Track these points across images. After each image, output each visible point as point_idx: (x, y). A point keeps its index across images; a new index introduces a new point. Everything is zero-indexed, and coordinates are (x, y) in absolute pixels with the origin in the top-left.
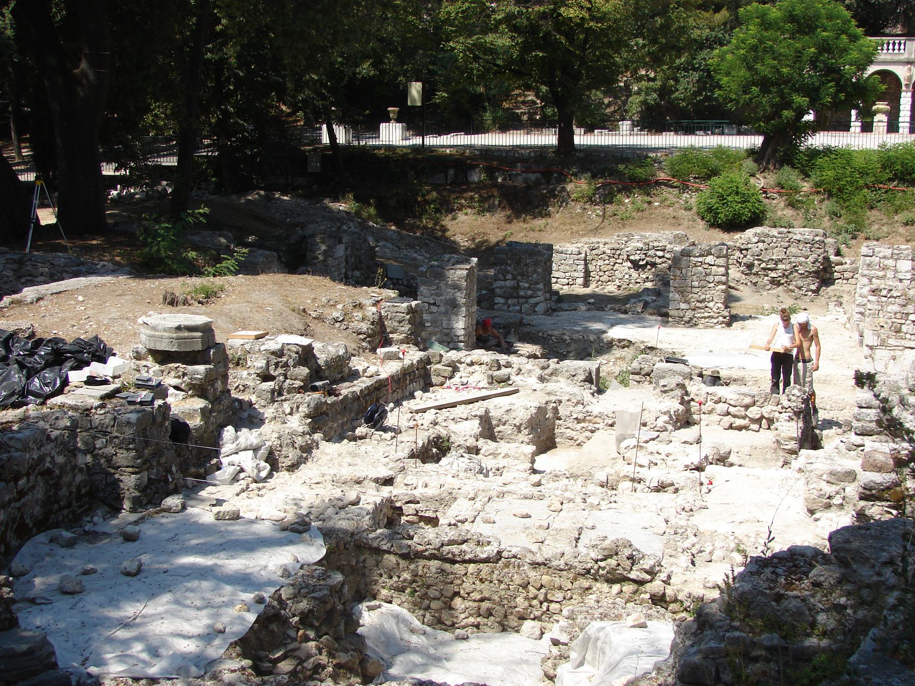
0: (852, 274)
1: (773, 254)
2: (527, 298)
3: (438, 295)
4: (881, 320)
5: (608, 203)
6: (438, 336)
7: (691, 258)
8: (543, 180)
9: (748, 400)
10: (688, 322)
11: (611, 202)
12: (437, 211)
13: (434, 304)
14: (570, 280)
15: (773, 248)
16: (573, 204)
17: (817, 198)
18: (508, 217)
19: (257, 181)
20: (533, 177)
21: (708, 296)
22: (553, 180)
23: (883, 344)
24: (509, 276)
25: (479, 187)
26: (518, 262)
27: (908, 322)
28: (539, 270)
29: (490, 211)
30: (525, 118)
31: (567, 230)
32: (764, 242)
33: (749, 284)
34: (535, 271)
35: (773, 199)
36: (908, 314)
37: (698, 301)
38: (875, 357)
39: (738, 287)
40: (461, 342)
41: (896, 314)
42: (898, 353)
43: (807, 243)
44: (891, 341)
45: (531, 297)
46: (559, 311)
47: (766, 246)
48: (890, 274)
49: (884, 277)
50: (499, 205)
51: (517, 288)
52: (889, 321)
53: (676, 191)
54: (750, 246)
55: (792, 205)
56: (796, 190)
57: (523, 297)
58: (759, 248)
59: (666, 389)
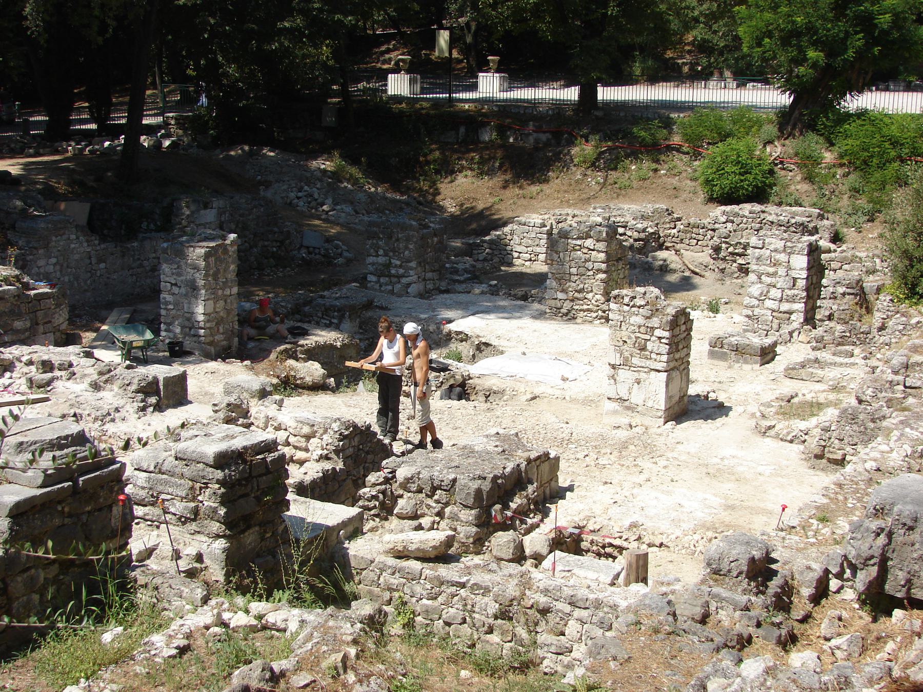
0: (840, 264)
1: (742, 237)
2: (399, 277)
3: (179, 275)
4: (624, 333)
5: (612, 170)
6: (180, 320)
7: (569, 241)
8: (553, 141)
9: (306, 430)
10: (566, 314)
11: (615, 169)
12: (438, 172)
13: (176, 285)
14: (532, 255)
15: (743, 230)
16: (574, 169)
17: (840, 172)
18: (506, 181)
19: (278, 133)
20: (544, 137)
21: (586, 286)
22: (563, 142)
23: (626, 363)
24: (381, 252)
25: (490, 145)
26: (390, 237)
27: (653, 338)
28: (411, 247)
29: (489, 175)
30: (686, 69)
31: (558, 198)
32: (733, 222)
33: (716, 270)
34: (407, 248)
35: (791, 171)
36: (653, 329)
37: (576, 291)
38: (618, 379)
39: (703, 273)
40: (202, 328)
41: (639, 327)
42: (643, 376)
43: (781, 226)
44: (636, 361)
45: (403, 276)
46: (452, 293)
47: (735, 227)
48: (782, 271)
49: (774, 274)
50: (500, 167)
51: (388, 265)
52: (633, 336)
53: (686, 158)
54: (717, 226)
55: (809, 178)
56: (817, 162)
57: (394, 276)
58: (728, 229)
59: (217, 408)
